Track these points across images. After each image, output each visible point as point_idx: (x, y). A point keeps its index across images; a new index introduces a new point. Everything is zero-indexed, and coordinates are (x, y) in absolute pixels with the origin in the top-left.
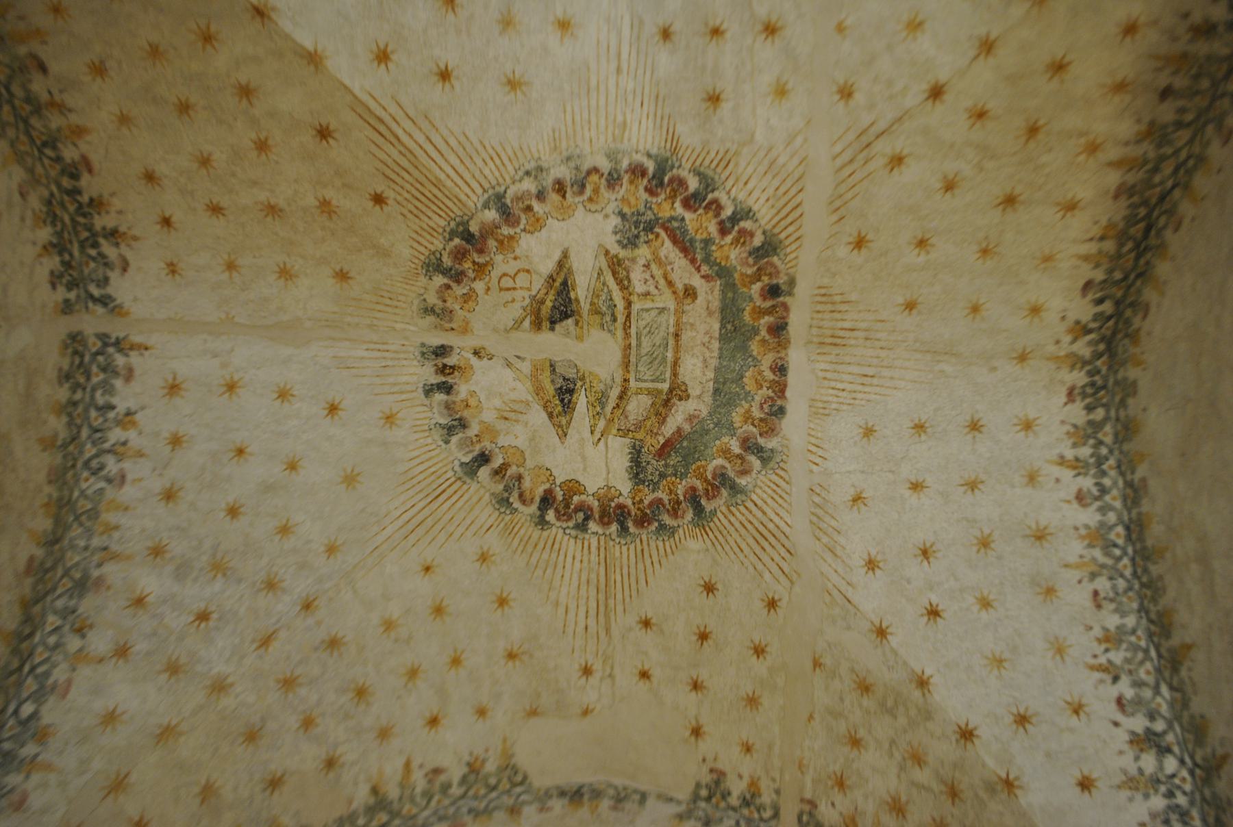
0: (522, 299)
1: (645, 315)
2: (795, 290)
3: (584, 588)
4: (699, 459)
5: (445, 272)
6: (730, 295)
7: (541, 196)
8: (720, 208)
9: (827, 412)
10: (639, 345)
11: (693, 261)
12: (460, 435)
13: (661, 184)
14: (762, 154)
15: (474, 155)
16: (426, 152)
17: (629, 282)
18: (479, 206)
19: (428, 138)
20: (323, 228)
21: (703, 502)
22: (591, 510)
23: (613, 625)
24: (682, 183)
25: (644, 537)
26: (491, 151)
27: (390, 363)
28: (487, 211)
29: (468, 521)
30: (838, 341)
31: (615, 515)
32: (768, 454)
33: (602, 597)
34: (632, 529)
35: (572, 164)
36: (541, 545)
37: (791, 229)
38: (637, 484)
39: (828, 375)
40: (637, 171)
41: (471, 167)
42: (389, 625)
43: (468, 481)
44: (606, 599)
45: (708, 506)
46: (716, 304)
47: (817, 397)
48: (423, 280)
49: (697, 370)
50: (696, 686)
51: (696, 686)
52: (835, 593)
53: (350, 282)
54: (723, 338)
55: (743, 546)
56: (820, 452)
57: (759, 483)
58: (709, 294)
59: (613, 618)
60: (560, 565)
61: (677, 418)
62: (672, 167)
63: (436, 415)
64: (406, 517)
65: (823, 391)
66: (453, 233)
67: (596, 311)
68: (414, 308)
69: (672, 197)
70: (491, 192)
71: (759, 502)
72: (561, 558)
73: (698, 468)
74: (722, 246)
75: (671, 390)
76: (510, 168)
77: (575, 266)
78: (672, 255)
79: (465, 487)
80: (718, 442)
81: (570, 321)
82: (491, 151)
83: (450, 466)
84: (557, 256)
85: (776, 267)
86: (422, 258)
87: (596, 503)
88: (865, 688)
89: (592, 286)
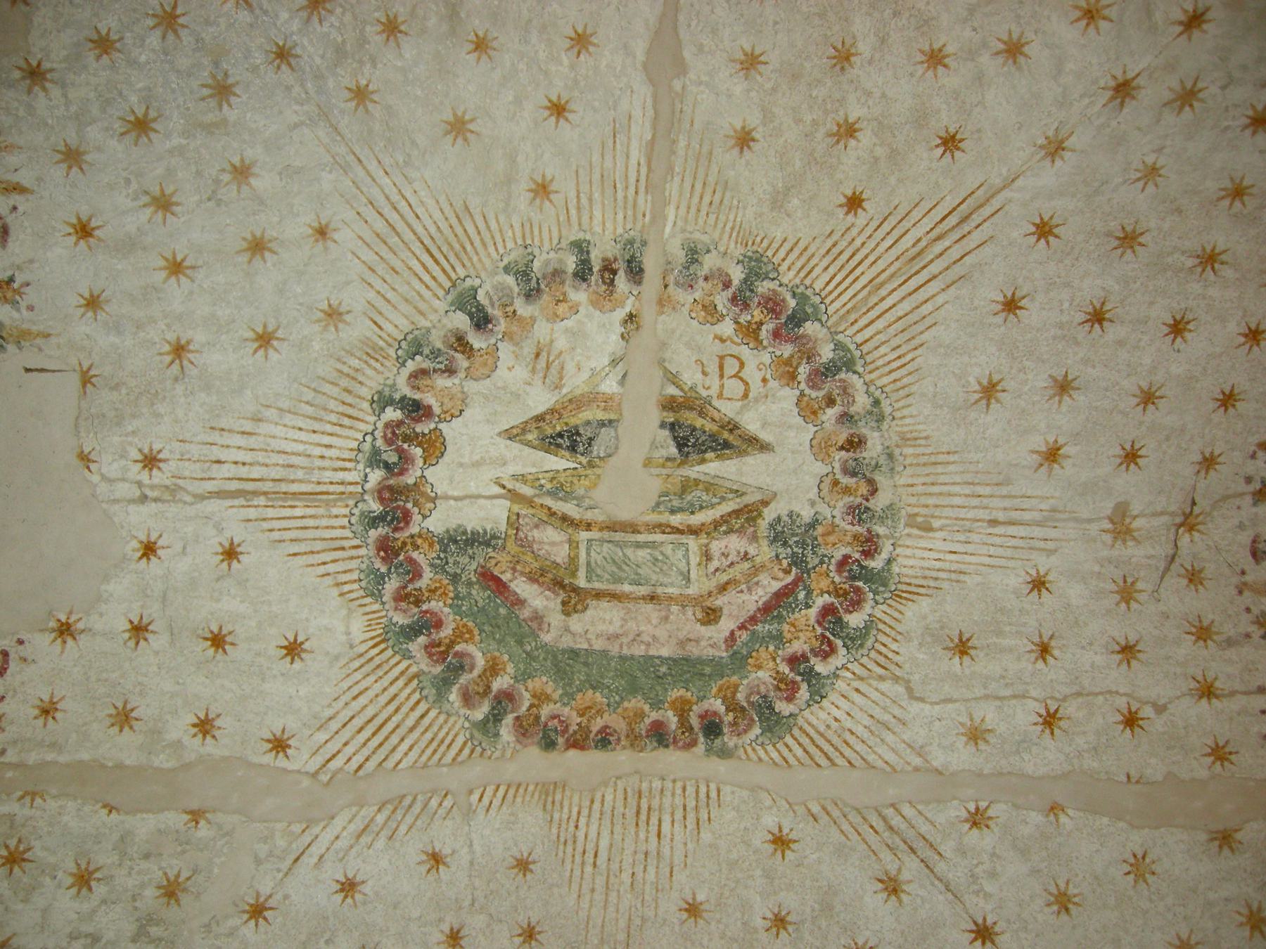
0: (708, 386)
1: (680, 554)
2: (715, 758)
3: (281, 459)
4: (481, 631)
5: (748, 282)
6: (708, 670)
7: (845, 418)
8: (825, 656)
9: (549, 807)
10: (638, 545)
11: (753, 619)
12: (516, 289)
13: (853, 578)
14: (897, 712)
15: (907, 335)
16: (917, 273)
17: (726, 533)
18: (840, 337)
19: (935, 277)
20: (815, 123)
21: (422, 640)
22: (401, 473)
23: (229, 503)
24: (856, 604)
25: (363, 551)
26: (909, 357)
27: (620, 194)
28: (832, 346)
29: (390, 295)
30: (643, 817)
31: (396, 505)
32: (492, 730)
33: (268, 486)
34: (374, 534)
35: (882, 460)
36: (349, 399)
37: (799, 752)
38: (441, 541)
39: (597, 805)
40: (869, 546)
41: (892, 330)
42: (242, 172)
43: (450, 298)
44: (265, 493)
45: (417, 646)
46: (694, 651)
47: (568, 793)
48: (738, 251)
49: (597, 625)
50: (139, 630)
51: (139, 630)
52: (307, 838)
53: (736, 151)
54: (648, 661)
55: (362, 700)
56: (496, 802)
57: (452, 720)
58: (710, 641)
59: (236, 502)
60: (317, 426)
61: (536, 598)
62: (876, 593)
63: (544, 256)
64: (403, 206)
65: (576, 799)
66: (802, 299)
67: (687, 486)
68: (697, 236)
69: (836, 592)
70: (857, 354)
71: (426, 721)
72: (329, 428)
73: (470, 632)
74: (774, 659)
75: (576, 590)
76: (885, 380)
77: (749, 460)
78: (760, 592)
79: (441, 293)
80: (506, 657)
81: (673, 450)
82: (909, 357)
83: (473, 273)
84: (765, 436)
85: (745, 731)
86: (769, 253)
87: (411, 481)
88: (171, 891)
89: (720, 482)
